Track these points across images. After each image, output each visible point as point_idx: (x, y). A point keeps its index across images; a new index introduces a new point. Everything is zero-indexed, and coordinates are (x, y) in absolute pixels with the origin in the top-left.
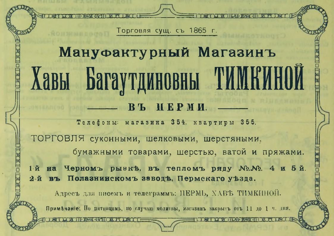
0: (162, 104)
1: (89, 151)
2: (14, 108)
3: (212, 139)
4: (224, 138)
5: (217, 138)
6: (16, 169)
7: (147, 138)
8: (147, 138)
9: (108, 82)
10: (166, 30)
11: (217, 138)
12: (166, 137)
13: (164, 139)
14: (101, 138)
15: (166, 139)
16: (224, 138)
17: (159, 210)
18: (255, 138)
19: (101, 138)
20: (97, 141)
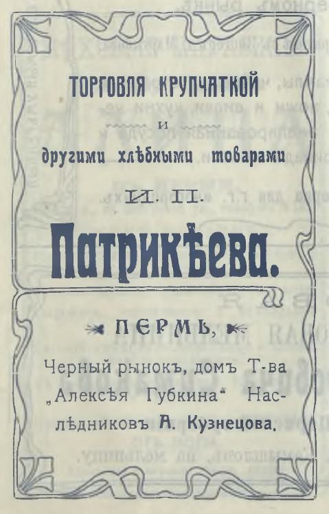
0: (205, 96)
1: (264, 393)
2: (123, 24)
3: (81, 395)
4: (103, 393)
5: (69, 365)
6: (277, 39)
7: (147, 320)
8: (147, 320)
9: (267, 253)
10: (223, 95)
11: (69, 365)
12: (94, 393)
13: (179, 397)
14: (92, 395)
15: (182, 397)
16: (103, 393)
17: (251, 151)
18: (194, 400)
19: (92, 395)
20: (162, 401)
